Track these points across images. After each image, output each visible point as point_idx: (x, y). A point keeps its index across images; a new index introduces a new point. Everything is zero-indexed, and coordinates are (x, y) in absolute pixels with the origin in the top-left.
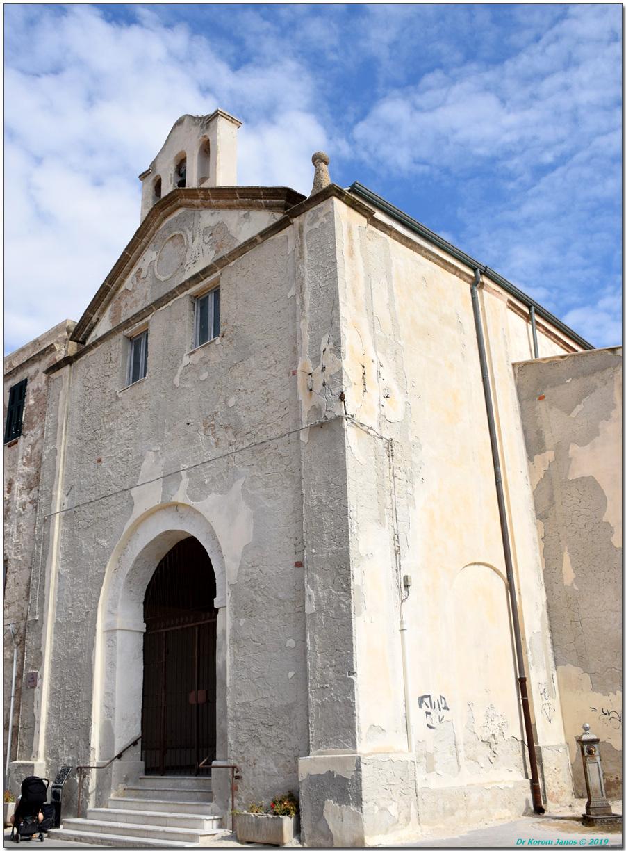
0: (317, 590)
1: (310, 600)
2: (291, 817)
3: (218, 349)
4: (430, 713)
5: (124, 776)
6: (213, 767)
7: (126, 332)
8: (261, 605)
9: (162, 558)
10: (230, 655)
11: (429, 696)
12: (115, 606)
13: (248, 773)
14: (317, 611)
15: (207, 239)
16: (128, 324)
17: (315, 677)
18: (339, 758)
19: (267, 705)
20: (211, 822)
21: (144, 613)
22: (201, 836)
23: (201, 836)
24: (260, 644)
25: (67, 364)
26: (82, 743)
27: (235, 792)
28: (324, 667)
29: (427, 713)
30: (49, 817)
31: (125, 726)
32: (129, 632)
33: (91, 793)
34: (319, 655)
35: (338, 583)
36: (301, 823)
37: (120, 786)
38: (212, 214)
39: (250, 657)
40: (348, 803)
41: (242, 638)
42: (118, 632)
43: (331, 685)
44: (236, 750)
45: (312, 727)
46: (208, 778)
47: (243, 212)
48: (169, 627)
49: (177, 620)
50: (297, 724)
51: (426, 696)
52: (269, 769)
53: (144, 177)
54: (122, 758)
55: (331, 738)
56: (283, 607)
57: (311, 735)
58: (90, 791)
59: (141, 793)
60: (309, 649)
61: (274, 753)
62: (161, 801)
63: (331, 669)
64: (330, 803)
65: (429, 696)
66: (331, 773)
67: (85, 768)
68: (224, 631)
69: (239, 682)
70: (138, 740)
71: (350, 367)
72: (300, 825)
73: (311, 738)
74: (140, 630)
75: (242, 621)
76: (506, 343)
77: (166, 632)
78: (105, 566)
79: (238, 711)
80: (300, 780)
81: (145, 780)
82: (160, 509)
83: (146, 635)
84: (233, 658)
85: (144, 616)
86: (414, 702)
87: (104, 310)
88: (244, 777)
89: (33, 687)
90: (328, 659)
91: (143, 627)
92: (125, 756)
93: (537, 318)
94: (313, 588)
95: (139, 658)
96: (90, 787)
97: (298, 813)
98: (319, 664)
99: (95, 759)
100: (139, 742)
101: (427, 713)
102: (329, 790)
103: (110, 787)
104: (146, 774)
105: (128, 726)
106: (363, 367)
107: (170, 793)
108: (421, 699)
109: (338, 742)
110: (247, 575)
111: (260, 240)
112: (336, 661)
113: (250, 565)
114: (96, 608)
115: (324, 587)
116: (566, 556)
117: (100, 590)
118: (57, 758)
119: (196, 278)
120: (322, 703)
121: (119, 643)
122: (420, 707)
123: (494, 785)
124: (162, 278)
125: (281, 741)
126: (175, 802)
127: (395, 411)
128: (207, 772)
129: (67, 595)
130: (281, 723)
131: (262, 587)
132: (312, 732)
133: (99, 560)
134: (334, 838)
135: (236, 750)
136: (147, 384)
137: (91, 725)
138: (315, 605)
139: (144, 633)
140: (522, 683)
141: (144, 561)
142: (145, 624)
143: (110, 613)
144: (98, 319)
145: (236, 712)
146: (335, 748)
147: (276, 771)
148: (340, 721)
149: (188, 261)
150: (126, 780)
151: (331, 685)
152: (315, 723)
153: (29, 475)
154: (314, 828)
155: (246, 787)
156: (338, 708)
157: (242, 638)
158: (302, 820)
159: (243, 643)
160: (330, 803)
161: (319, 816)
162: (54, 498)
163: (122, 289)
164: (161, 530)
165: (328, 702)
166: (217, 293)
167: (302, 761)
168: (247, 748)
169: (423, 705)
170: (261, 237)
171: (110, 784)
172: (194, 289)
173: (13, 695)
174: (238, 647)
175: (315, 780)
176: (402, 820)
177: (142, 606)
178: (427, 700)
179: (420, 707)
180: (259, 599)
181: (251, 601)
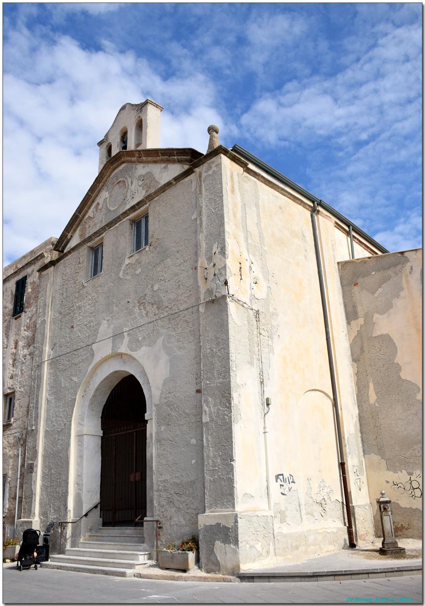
0: (210, 407)
1: (206, 413)
2: (193, 553)
3: (148, 254)
4: (283, 486)
7: (89, 244)
8: (174, 418)
11: (282, 475)
12: (83, 420)
13: (167, 524)
15: (140, 183)
16: (90, 239)
17: (209, 463)
18: (224, 514)
19: (178, 481)
20: (143, 556)
22: (137, 565)
23: (137, 565)
25: (52, 266)
26: (62, 507)
28: (215, 457)
29: (281, 485)
31: (89, 497)
34: (211, 449)
38: (144, 167)
40: (230, 543)
43: (219, 468)
44: (159, 511)
47: (163, 165)
51: (280, 475)
52: (180, 522)
53: (101, 144)
55: (219, 502)
56: (188, 419)
57: (206, 500)
59: (100, 538)
63: (219, 458)
64: (218, 544)
65: (282, 475)
66: (218, 524)
68: (151, 435)
70: (97, 505)
71: (231, 264)
73: (206, 502)
75: (163, 428)
76: (333, 250)
77: (115, 436)
83: (103, 439)
84: (157, 451)
86: (272, 479)
87: (75, 230)
89: (31, 472)
90: (217, 452)
92: (90, 515)
93: (353, 233)
95: (98, 452)
96: (68, 535)
98: (211, 454)
100: (99, 506)
101: (281, 485)
104: (103, 526)
105: (91, 496)
106: (240, 263)
108: (277, 477)
109: (223, 504)
111: (174, 183)
112: (222, 452)
113: (167, 392)
115: (215, 405)
116: (371, 385)
117: (73, 410)
118: (47, 517)
119: (133, 209)
122: (277, 481)
123: (324, 530)
124: (112, 209)
127: (261, 292)
129: (52, 413)
130: (187, 492)
136: (103, 277)
140: (342, 466)
144: (71, 236)
149: (129, 198)
150: (91, 530)
151: (219, 468)
152: (209, 493)
154: (208, 559)
160: (218, 544)
161: (211, 551)
163: (87, 217)
164: (111, 371)
166: (147, 217)
167: (200, 517)
169: (279, 480)
170: (175, 181)
171: (80, 533)
172: (132, 216)
173: (19, 477)
175: (209, 529)
176: (264, 554)
177: (100, 419)
178: (281, 477)
179: (277, 481)
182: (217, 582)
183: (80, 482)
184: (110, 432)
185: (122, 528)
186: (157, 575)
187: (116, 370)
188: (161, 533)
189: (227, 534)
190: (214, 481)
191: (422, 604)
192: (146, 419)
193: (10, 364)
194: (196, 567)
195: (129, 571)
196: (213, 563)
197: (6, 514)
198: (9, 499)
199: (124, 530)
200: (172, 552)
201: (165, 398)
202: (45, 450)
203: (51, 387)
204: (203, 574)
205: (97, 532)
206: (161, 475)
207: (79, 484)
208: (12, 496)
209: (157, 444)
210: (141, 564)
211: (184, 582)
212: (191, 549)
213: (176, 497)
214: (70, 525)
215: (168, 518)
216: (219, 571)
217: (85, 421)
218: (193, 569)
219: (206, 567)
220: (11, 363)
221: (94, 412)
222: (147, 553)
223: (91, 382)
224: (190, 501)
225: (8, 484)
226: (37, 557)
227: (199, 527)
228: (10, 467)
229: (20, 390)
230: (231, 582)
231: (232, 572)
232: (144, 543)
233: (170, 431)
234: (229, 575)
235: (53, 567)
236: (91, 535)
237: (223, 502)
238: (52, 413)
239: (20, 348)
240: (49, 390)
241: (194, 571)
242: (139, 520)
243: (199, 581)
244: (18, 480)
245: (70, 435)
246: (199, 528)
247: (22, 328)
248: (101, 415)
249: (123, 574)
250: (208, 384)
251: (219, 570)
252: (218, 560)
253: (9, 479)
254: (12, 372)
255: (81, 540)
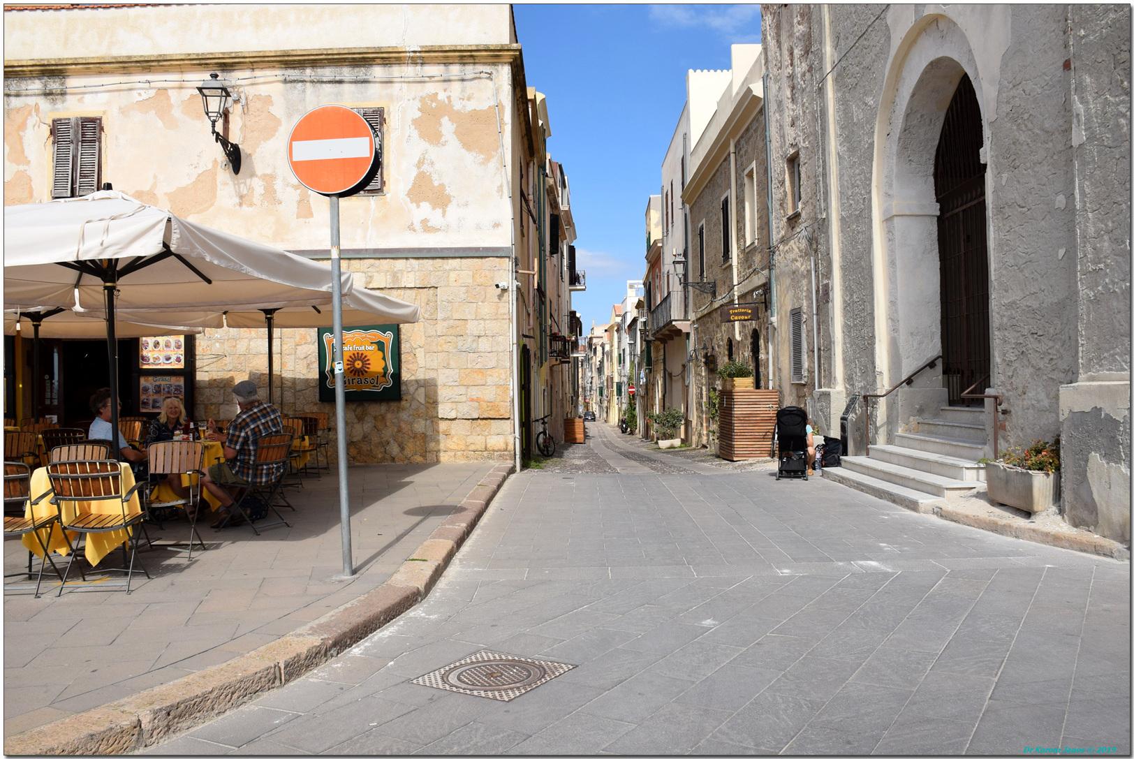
0: (1087, 102)
1: (1079, 121)
2: (1048, 475)
5: (918, 407)
6: (986, 397)
8: (1025, 147)
9: (948, 106)
10: (994, 232)
12: (891, 186)
13: (1018, 406)
14: (1087, 139)
17: (1085, 252)
18: (1108, 386)
19: (1035, 305)
20: (975, 471)
21: (936, 190)
22: (947, 489)
23: (947, 489)
24: (1025, 209)
26: (869, 366)
27: (1001, 433)
28: (1098, 236)
30: (834, 453)
31: (915, 344)
32: (914, 218)
33: (880, 427)
34: (1090, 215)
35: (1117, 81)
36: (1062, 484)
37: (912, 418)
39: (1015, 231)
40: (1118, 460)
41: (1006, 204)
42: (896, 220)
43: (1107, 266)
44: (1004, 373)
45: (1082, 336)
46: (979, 409)
48: (966, 203)
49: (974, 193)
50: (1071, 331)
52: (1038, 401)
54: (912, 384)
55: (1106, 354)
56: (1051, 144)
57: (1080, 349)
58: (878, 425)
59: (933, 428)
60: (1078, 207)
61: (1045, 377)
62: (938, 440)
63: (1106, 237)
64: (1095, 457)
66: (1097, 410)
67: (872, 396)
68: (1101, 505)
69: (1004, 272)
70: (936, 359)
72: (1060, 487)
73: (1080, 354)
74: (930, 213)
75: (1005, 176)
77: (964, 211)
78: (873, 132)
79: (1004, 316)
80: (1061, 420)
81: (947, 413)
82: (919, 34)
83: (940, 220)
84: (997, 236)
85: (936, 194)
88: (1012, 410)
89: (828, 302)
90: (1102, 221)
91: (935, 209)
92: (918, 382)
94: (1083, 101)
95: (932, 251)
96: (878, 419)
97: (1058, 469)
98: (1091, 230)
99: (884, 383)
102: (1095, 437)
103: (898, 420)
104: (950, 405)
105: (920, 343)
107: (958, 429)
109: (1115, 360)
110: (1008, 102)
112: (1113, 222)
113: (1011, 86)
114: (870, 192)
115: (1098, 94)
117: (872, 166)
118: (853, 385)
120: (1095, 295)
121: (897, 234)
125: (1052, 359)
126: (949, 442)
128: (980, 402)
129: (847, 181)
130: (1051, 331)
131: (1026, 116)
132: (1082, 345)
133: (868, 126)
134: (1098, 512)
135: (1004, 373)
137: (875, 344)
138: (1086, 130)
139: (939, 218)
141: (919, 116)
142: (938, 204)
143: (888, 195)
145: (1002, 316)
146: (1110, 370)
147: (1047, 406)
148: (1117, 324)
150: (921, 411)
151: (1107, 266)
152: (1085, 329)
153: (804, 36)
154: (1076, 493)
155: (1015, 427)
156: (1115, 304)
157: (1006, 204)
158: (1063, 480)
159: (1007, 211)
160: (1095, 457)
161: (1082, 477)
162: (824, 55)
164: (924, 64)
165: (1102, 294)
167: (1065, 391)
168: (1015, 369)
171: (898, 417)
173: (815, 312)
174: (1003, 219)
175: (1079, 418)
177: (932, 180)
180: (1022, 138)
181: (1014, 143)
182: (1081, 551)
183: (895, 315)
184: (969, 198)
185: (956, 408)
186: (967, 516)
187: (932, 59)
188: (1007, 424)
189: (1114, 437)
190: (1096, 301)
191: (1130, 756)
192: (982, 162)
193: (789, 99)
194: (1054, 509)
195: (925, 500)
196: (1085, 505)
197: (806, 379)
198: (807, 353)
199: (977, 414)
200: (1005, 469)
201: (1008, 102)
202: (843, 257)
203: (842, 128)
204: (1063, 527)
205: (936, 415)
206: (1006, 291)
207: (893, 319)
208: (811, 348)
209: (997, 219)
210: (960, 489)
211: (1014, 539)
212: (1041, 467)
213: (1032, 343)
214: (882, 401)
215: (1020, 390)
216: (1095, 527)
217: (894, 186)
218: (1044, 514)
219: (1074, 513)
220: (790, 96)
221: (914, 165)
222: (982, 465)
223: (897, 99)
224: (1058, 351)
225: (805, 326)
226: (38, 465)
227: (1061, 415)
228: (804, 294)
229: (804, 145)
230: (1112, 557)
231: (1120, 532)
232: (985, 444)
233: (1019, 182)
234: (1114, 539)
235: (842, 480)
236: (921, 420)
237: (1113, 355)
238: (847, 181)
239: (796, 61)
240: (841, 135)
241: (1049, 520)
242: (968, 393)
243: (1043, 542)
244: (815, 316)
245: (871, 220)
246: (1062, 418)
247: (795, 21)
248: (932, 170)
249: (913, 505)
250: (1084, 37)
251: (1096, 524)
252: (1093, 499)
253: (805, 316)
254: (791, 113)
255: (900, 430)
